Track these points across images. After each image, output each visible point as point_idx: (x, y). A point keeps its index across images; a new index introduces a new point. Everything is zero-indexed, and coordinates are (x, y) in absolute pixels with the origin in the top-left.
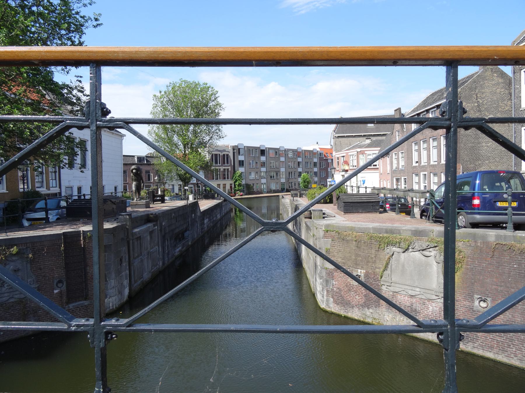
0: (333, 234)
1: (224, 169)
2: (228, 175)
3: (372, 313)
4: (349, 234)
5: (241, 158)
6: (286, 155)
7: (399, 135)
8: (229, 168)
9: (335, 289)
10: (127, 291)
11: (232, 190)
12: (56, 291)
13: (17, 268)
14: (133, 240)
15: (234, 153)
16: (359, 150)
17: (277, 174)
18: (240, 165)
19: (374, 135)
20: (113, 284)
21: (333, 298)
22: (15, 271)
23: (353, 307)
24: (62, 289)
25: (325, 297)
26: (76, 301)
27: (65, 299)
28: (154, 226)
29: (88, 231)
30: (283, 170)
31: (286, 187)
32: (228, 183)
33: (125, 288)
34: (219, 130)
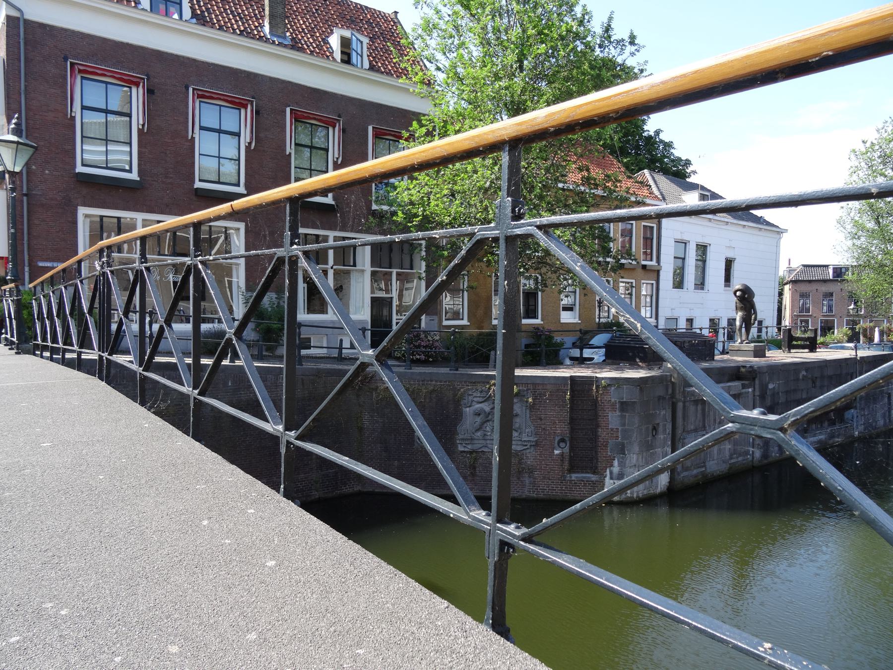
12: (556, 452)
14: (684, 402)
26: (583, 473)
27: (566, 465)
28: (744, 387)
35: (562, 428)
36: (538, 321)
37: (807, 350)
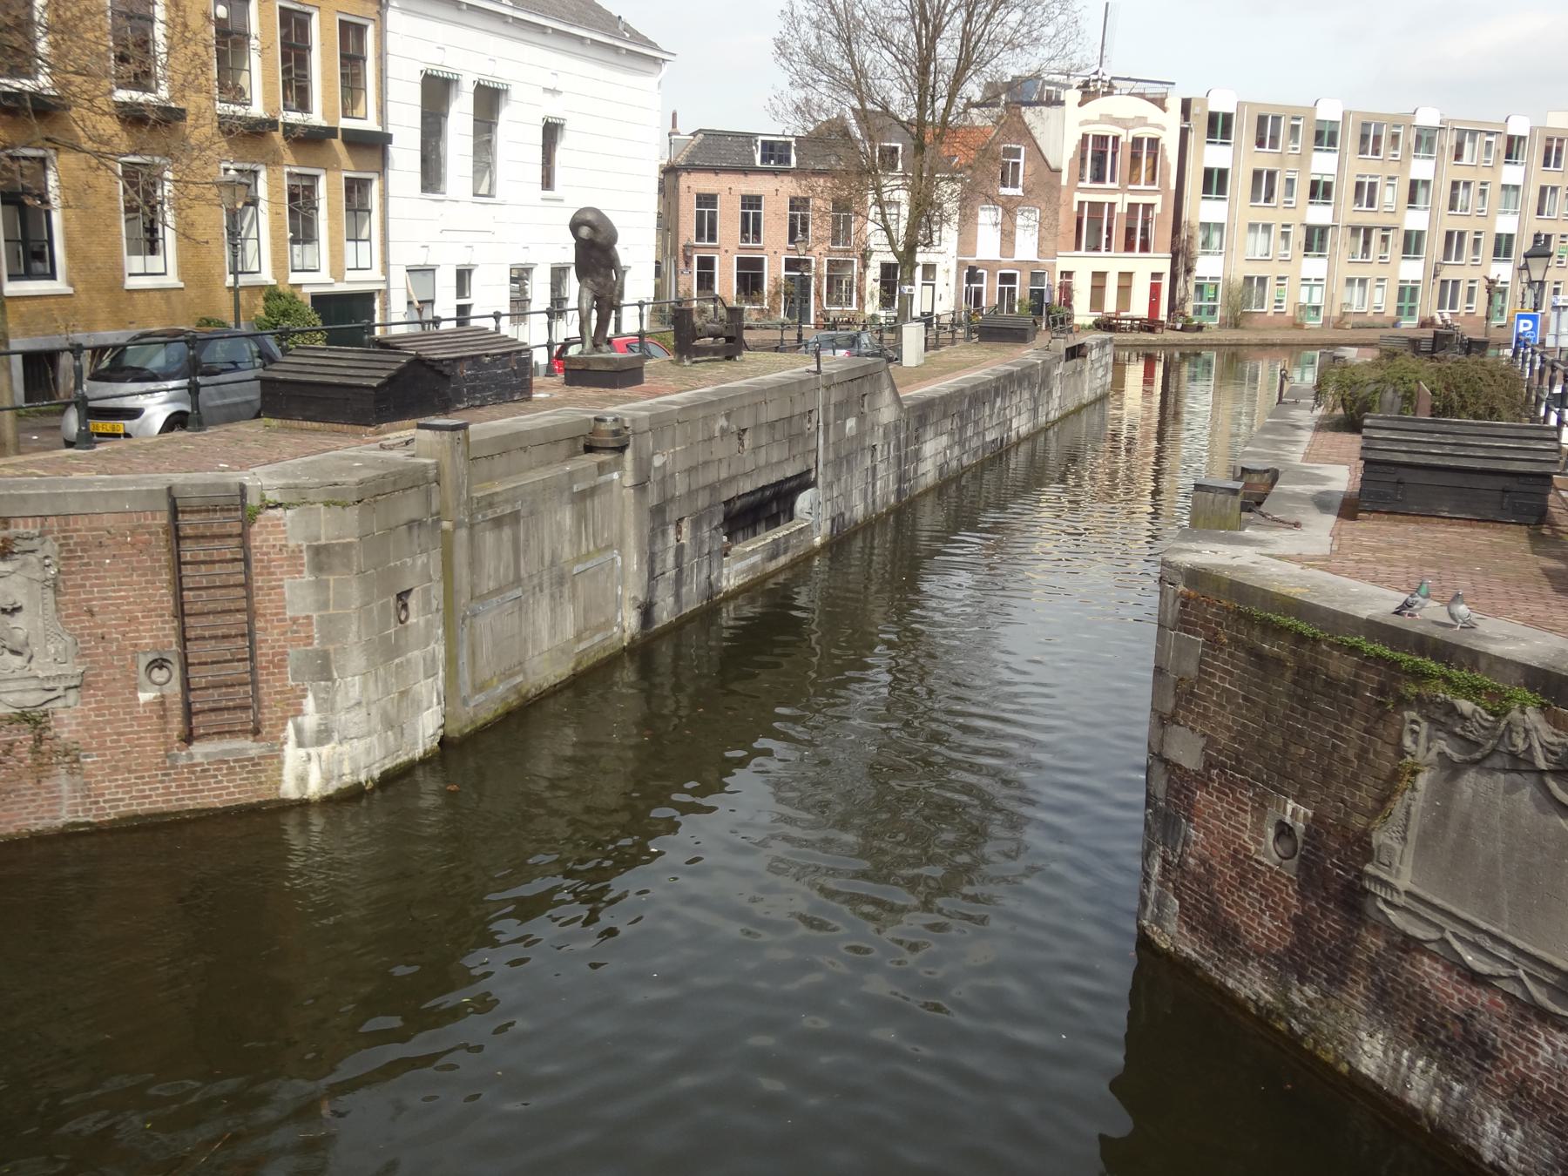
1: (1133, 207)
12: (144, 697)
13: (11, 600)
15: (1184, 133)
18: (1207, 188)
24: (167, 690)
27: (176, 725)
33: (418, 707)
36: (58, 286)
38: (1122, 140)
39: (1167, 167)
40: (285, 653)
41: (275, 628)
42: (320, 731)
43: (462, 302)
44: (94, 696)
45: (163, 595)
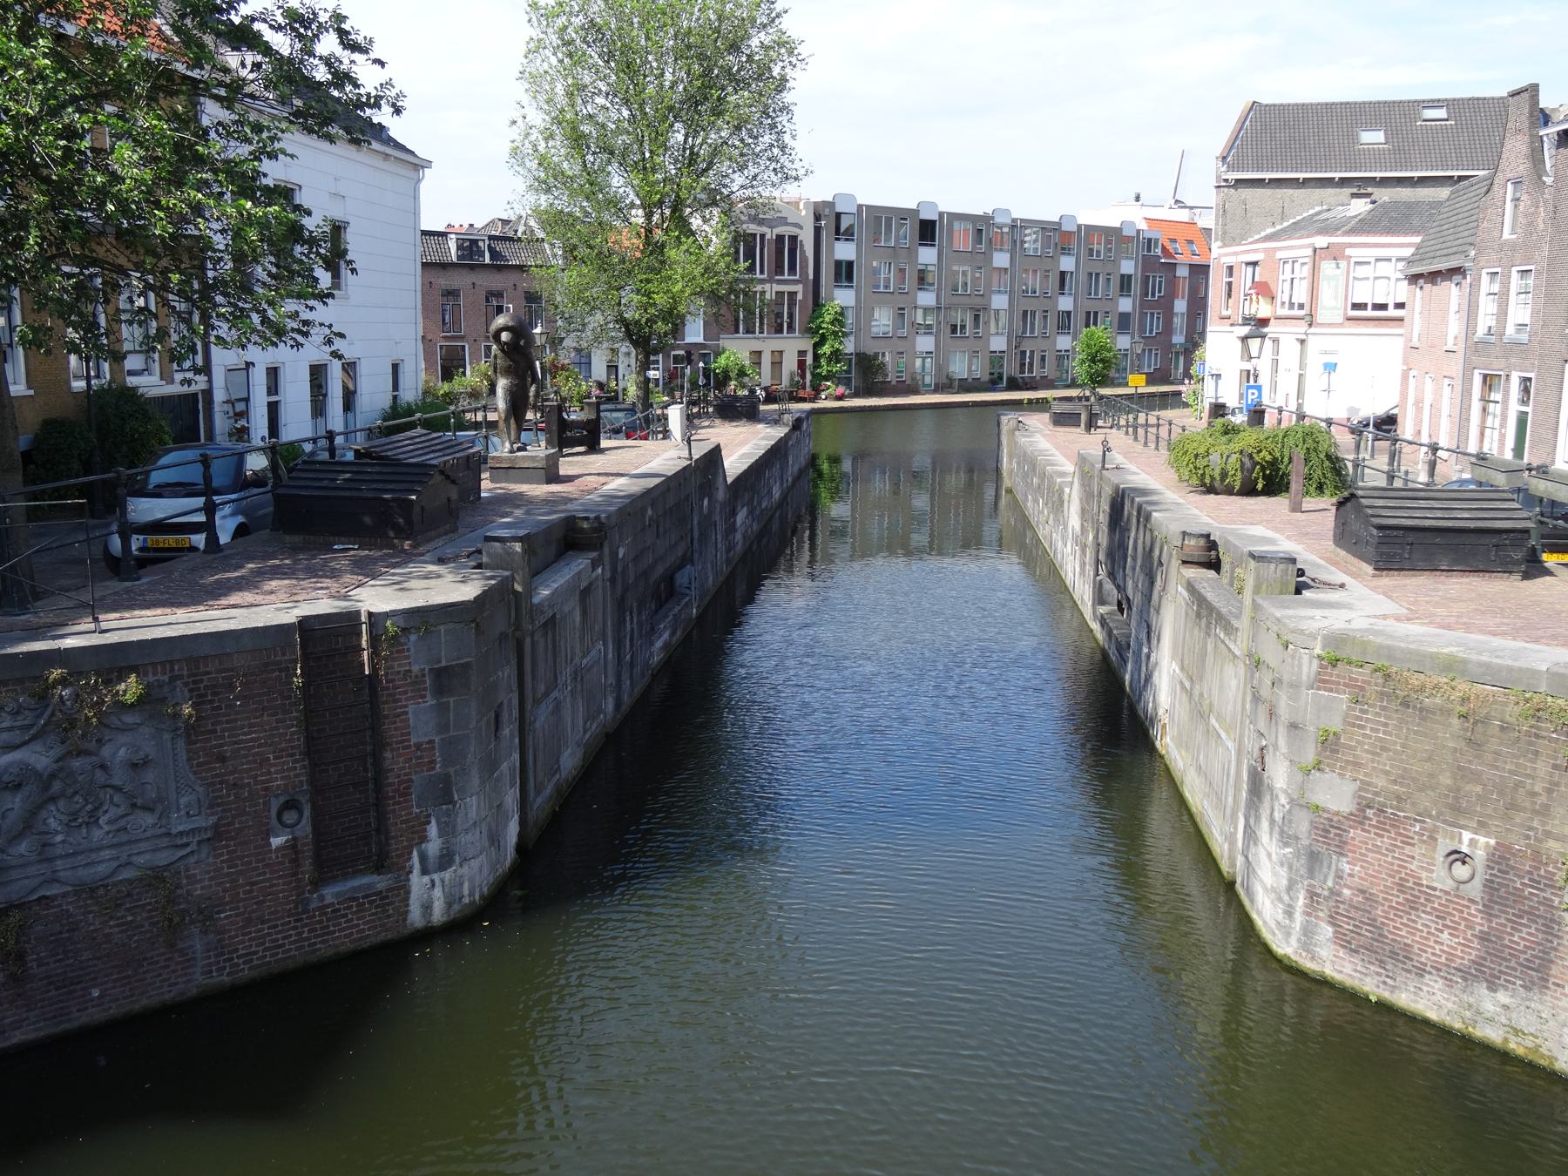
0: (1361, 674)
1: (780, 294)
2: (791, 316)
3: (1506, 1007)
4: (1436, 687)
5: (845, 251)
6: (1016, 245)
7: (1516, 200)
8: (799, 288)
9: (1347, 892)
10: (513, 830)
11: (803, 376)
12: (276, 842)
15: (818, 230)
16: (1321, 241)
17: (977, 317)
19: (1384, 182)
20: (473, 814)
21: (1334, 925)
22: (134, 766)
23: (1421, 972)
25: (1299, 917)
27: (307, 865)
28: (594, 566)
29: (387, 615)
30: (999, 302)
31: (1009, 369)
32: (793, 346)
33: (507, 819)
34: (783, 148)
35: (285, 772)
37: (581, 449)
38: (768, 237)
39: (804, 260)
40: (411, 781)
41: (400, 755)
42: (442, 856)
43: (273, 399)
44: (227, 846)
45: (293, 734)
